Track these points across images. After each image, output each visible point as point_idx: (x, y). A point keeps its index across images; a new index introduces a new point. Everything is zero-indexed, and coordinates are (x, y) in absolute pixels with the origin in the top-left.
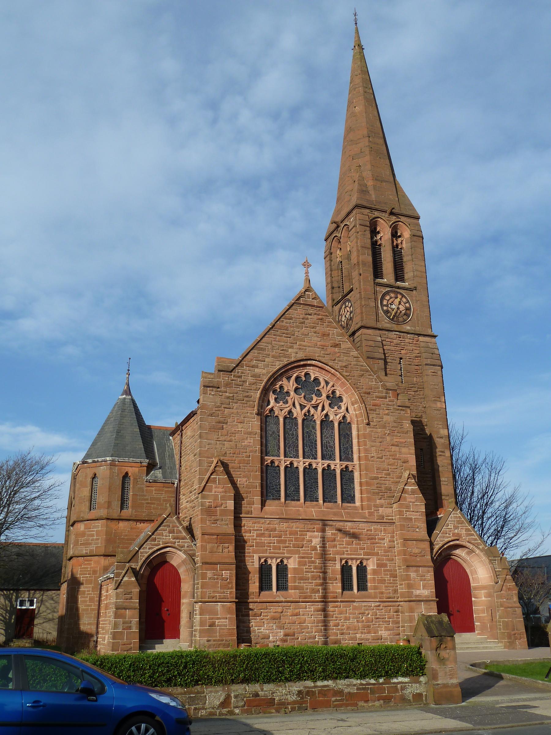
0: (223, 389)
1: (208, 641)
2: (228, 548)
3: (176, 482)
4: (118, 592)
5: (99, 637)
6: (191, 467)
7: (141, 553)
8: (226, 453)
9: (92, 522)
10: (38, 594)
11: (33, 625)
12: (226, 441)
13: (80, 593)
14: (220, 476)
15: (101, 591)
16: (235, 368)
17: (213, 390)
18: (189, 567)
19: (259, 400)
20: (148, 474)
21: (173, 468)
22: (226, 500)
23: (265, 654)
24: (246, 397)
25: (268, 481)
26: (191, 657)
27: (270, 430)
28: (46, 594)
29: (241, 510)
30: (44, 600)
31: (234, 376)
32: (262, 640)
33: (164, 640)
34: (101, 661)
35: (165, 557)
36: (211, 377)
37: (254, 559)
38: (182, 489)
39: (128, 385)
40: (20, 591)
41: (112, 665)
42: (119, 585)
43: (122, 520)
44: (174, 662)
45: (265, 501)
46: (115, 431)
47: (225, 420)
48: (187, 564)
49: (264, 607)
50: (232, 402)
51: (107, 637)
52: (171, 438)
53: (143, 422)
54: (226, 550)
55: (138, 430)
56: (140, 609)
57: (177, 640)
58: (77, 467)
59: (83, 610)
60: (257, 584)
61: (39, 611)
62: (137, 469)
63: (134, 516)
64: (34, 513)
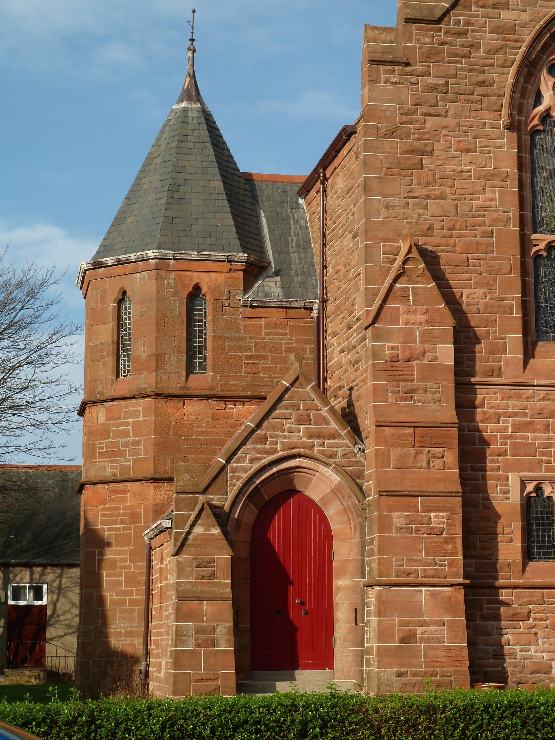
0: (418, 67)
1: (400, 675)
2: (442, 457)
3: (316, 307)
4: (181, 559)
5: (151, 663)
6: (348, 266)
7: (233, 471)
8: (430, 228)
9: (123, 403)
10: (51, 575)
11: (45, 640)
12: (430, 198)
13: (105, 565)
14: (417, 283)
15: (150, 561)
16: (447, 12)
17: (394, 71)
18: (349, 504)
19: (513, 91)
20: (247, 287)
21: (307, 273)
22: (435, 343)
23: (511, 707)
24: (478, 84)
25: (542, 295)
26: (317, 710)
27: (543, 168)
28: (69, 575)
29: (473, 366)
30: (63, 587)
31: (447, 33)
32: (533, 675)
33: (296, 672)
34: (92, 716)
35: (291, 480)
36: (389, 37)
37: (507, 485)
38: (331, 322)
39: (193, 76)
40: (11, 569)
41: (117, 725)
42: (183, 544)
43: (192, 397)
44: (275, 721)
45: (534, 345)
46: (166, 188)
47: (426, 145)
48: (343, 497)
49: (535, 599)
50: (443, 100)
51: (164, 662)
52: (301, 201)
53: (231, 165)
54: (438, 463)
55: (221, 184)
56: (234, 600)
57: (327, 672)
58: (84, 277)
59: (114, 602)
60: (518, 544)
61: (54, 610)
62: (220, 278)
63: (219, 388)
64: (21, 398)
